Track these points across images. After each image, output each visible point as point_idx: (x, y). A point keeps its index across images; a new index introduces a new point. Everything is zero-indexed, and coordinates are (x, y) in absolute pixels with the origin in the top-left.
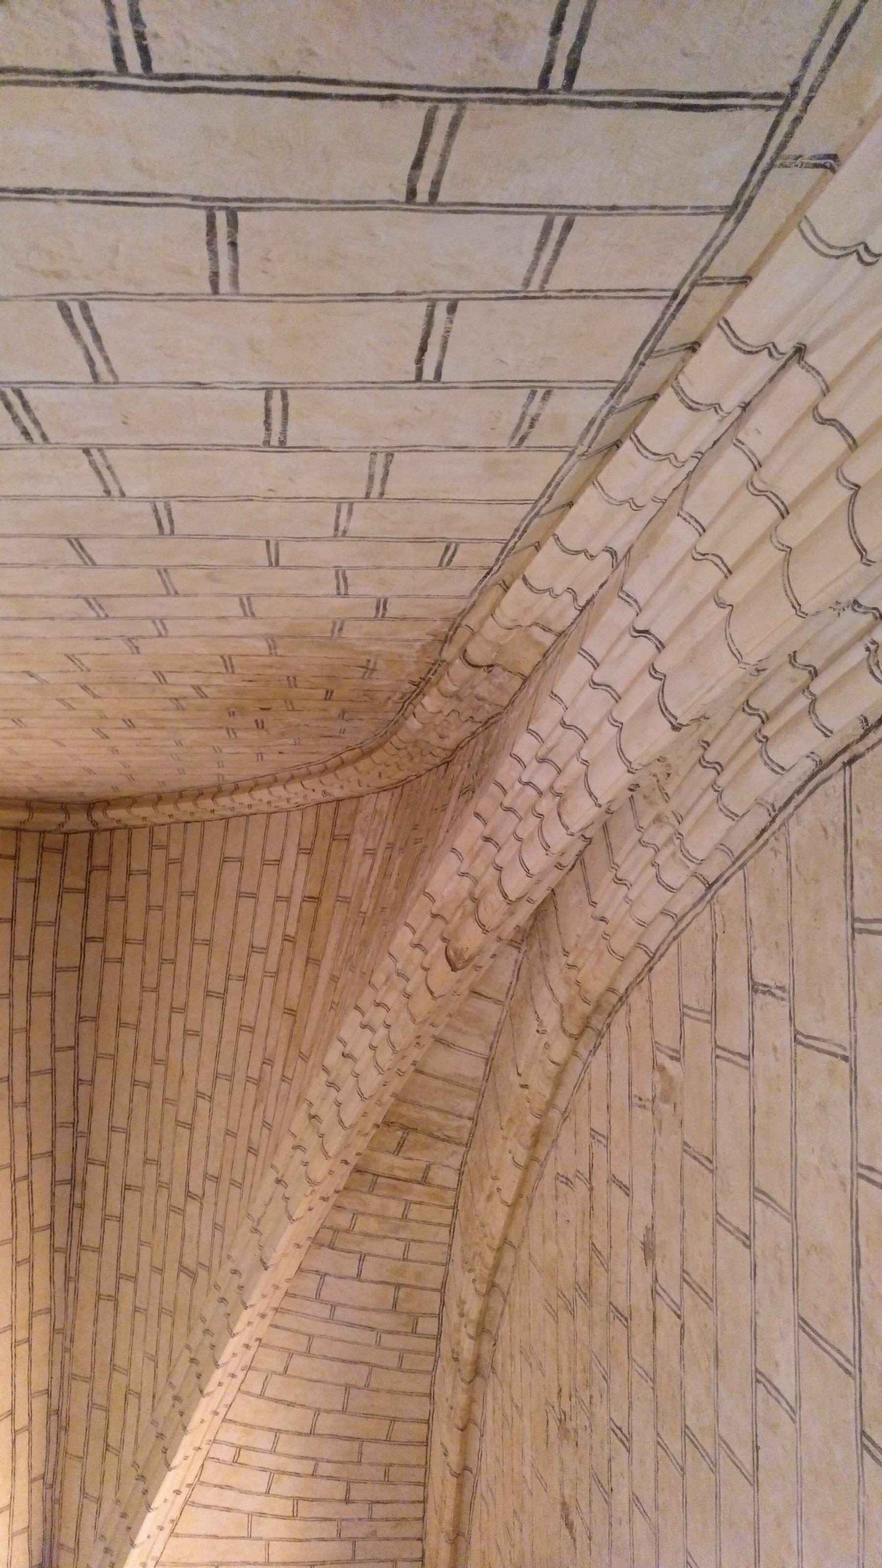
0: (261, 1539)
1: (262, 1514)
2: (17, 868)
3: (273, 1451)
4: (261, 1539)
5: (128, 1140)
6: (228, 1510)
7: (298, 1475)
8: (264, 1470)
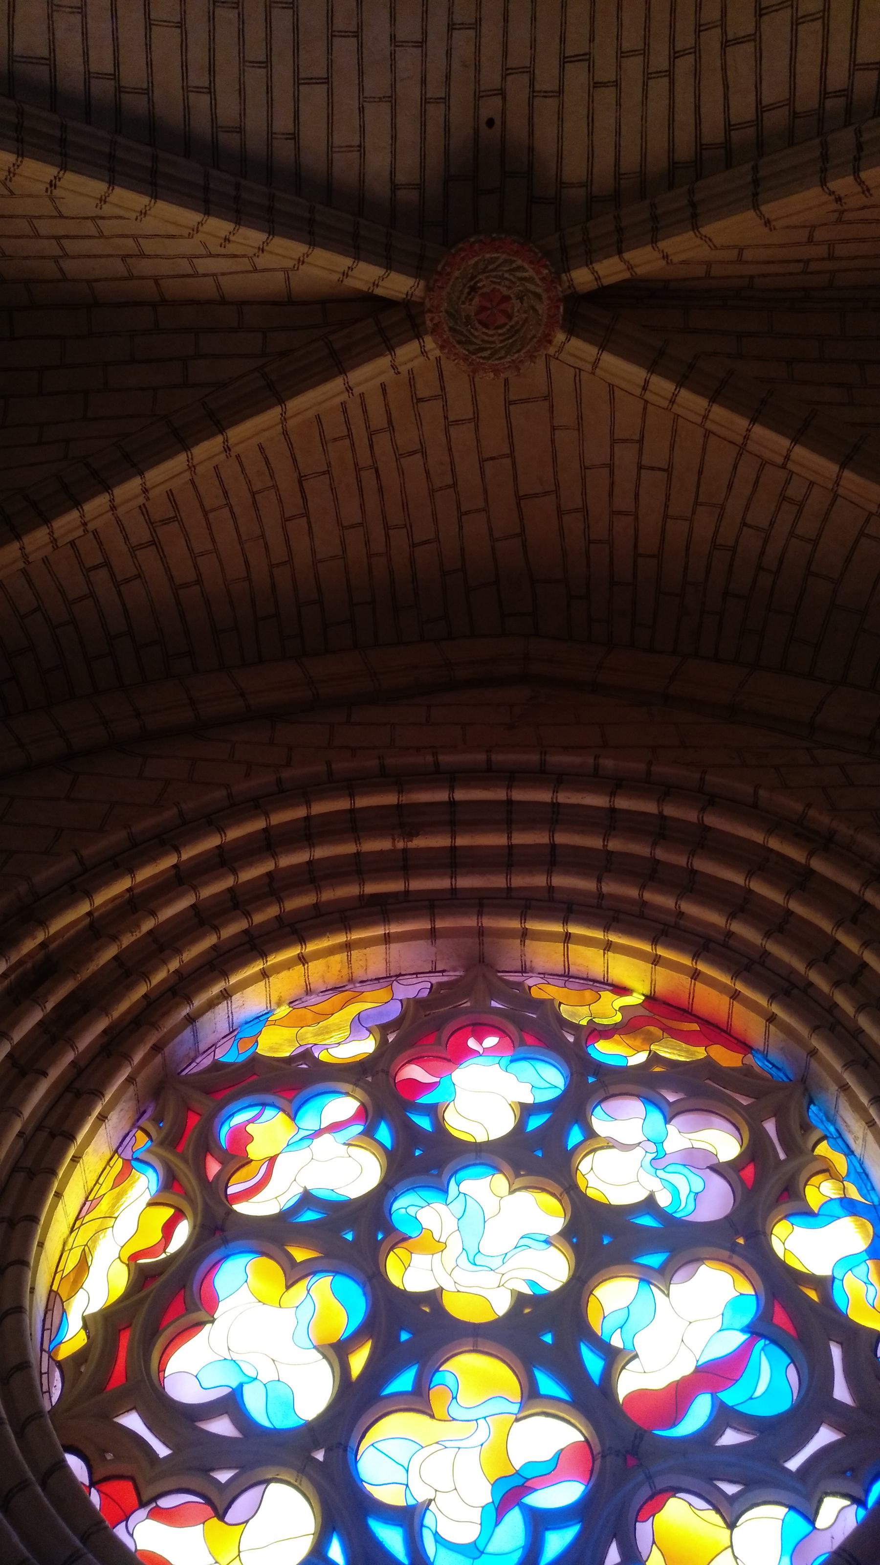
0: (694, 513)
1: (721, 517)
2: (113, 575)
3: (792, 534)
4: (694, 513)
5: (823, 77)
6: (730, 486)
7: (762, 553)
8: (772, 524)
